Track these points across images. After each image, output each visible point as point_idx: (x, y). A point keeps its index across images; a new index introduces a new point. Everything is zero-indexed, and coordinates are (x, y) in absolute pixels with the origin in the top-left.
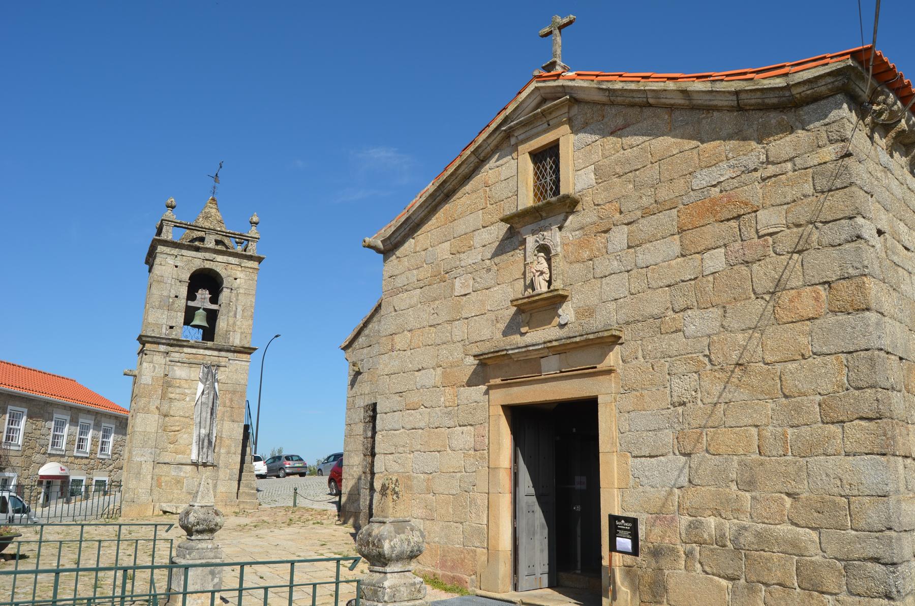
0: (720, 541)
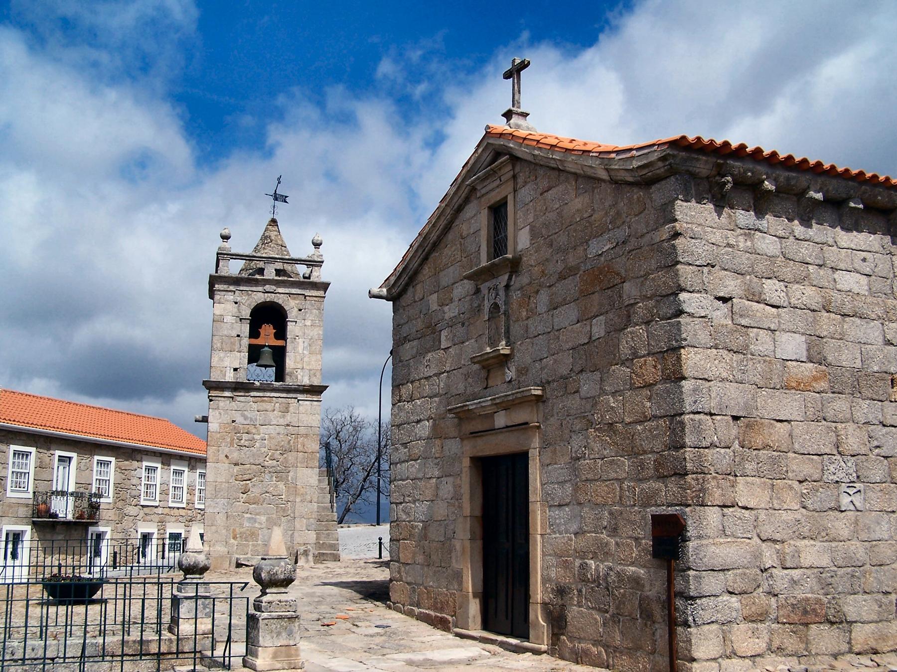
0: (596, 580)
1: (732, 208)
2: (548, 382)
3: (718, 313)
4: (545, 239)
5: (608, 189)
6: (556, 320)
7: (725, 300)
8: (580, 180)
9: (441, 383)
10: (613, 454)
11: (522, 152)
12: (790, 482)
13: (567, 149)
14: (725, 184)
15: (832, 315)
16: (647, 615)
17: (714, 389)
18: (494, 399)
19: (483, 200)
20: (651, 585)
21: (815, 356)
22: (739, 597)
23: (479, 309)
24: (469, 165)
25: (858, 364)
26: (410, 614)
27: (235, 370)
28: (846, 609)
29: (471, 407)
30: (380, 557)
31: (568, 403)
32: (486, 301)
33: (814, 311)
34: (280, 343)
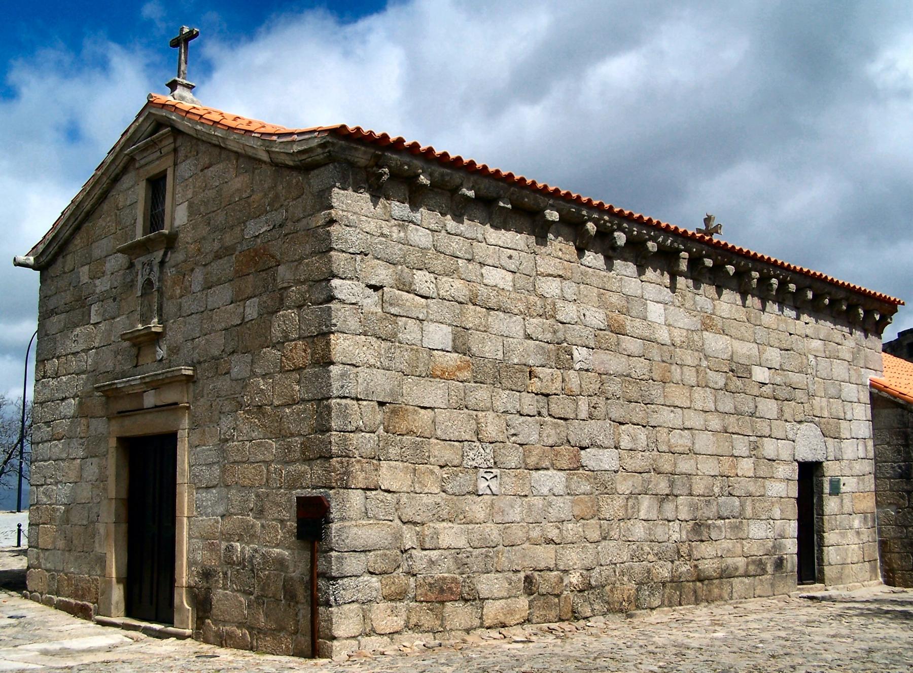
0: (241, 563)
1: (387, 199)
2: (199, 363)
3: (369, 300)
4: (203, 216)
5: (269, 171)
6: (210, 299)
7: (376, 288)
8: (241, 160)
9: (89, 360)
10: (261, 436)
11: (184, 125)
12: (431, 467)
13: (229, 127)
14: (382, 175)
15: (478, 308)
16: (291, 596)
17: (361, 374)
18: (144, 378)
19: (141, 171)
20: (295, 566)
21: (460, 347)
22: (380, 577)
23: (131, 285)
24: (129, 134)
25: (500, 356)
26: (48, 603)
28: (479, 587)
29: (119, 386)
30: (19, 545)
31: (219, 384)
32: (140, 276)
33: (461, 303)
34: (890, 334)
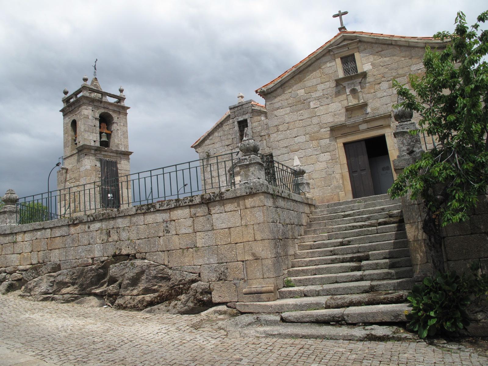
27: (95, 141)
